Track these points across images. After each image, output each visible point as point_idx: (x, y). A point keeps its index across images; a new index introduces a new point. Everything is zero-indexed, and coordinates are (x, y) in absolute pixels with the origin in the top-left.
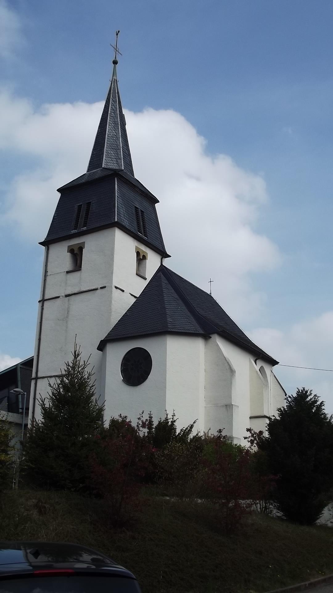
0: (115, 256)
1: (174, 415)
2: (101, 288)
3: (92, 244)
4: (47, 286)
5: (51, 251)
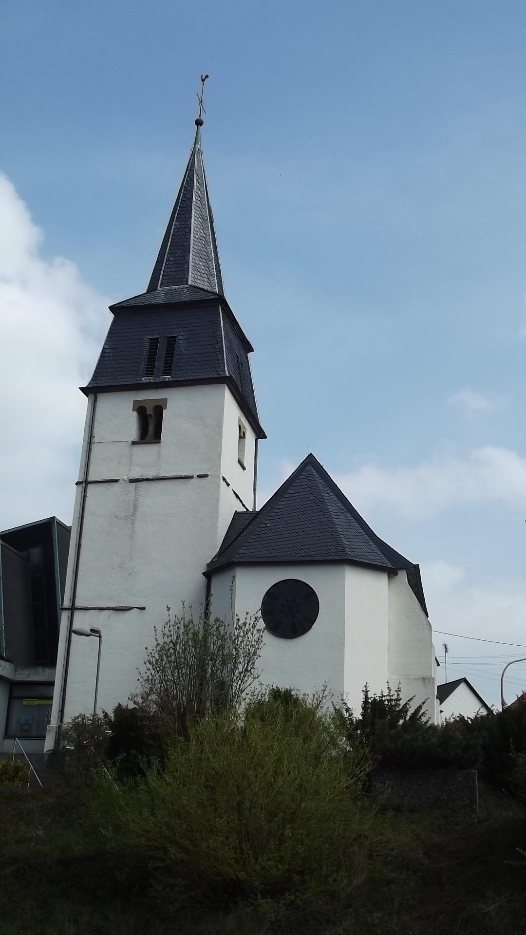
0: (224, 429)
1: (398, 691)
2: (199, 476)
3: (181, 407)
4: (92, 459)
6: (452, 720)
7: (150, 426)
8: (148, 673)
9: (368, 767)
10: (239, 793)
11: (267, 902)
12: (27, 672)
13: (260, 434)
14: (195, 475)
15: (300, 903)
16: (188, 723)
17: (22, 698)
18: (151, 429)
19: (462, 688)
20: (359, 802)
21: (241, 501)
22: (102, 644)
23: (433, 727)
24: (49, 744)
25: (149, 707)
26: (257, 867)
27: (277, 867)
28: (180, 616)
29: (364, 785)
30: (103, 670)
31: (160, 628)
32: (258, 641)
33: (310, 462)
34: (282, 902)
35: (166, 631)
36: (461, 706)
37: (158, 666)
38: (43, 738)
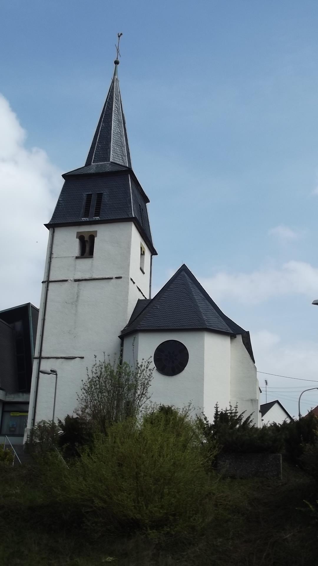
2: (117, 278)
3: (105, 236)
6: (269, 425)
7: (87, 248)
8: (83, 395)
9: (215, 452)
10: (137, 467)
11: (153, 532)
12: (13, 396)
13: (153, 252)
14: (114, 276)
15: (173, 533)
16: (107, 425)
17: (10, 412)
18: (87, 249)
19: (276, 407)
20: (209, 473)
21: (142, 293)
22: (58, 379)
23: (257, 429)
24: (25, 439)
25: (85, 417)
26: (147, 511)
27: (159, 511)
28: (102, 361)
29: (213, 463)
30: (57, 395)
31: (90, 369)
32: (150, 376)
33: (184, 269)
34: (163, 532)
35: (94, 370)
36: (275, 417)
37: (89, 391)
38: (22, 436)
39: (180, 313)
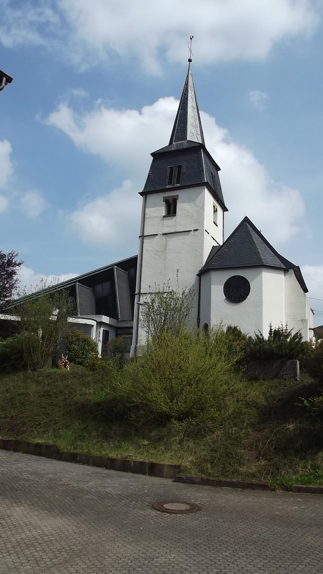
5: (148, 200)
13: (225, 209)
39: (243, 256)
